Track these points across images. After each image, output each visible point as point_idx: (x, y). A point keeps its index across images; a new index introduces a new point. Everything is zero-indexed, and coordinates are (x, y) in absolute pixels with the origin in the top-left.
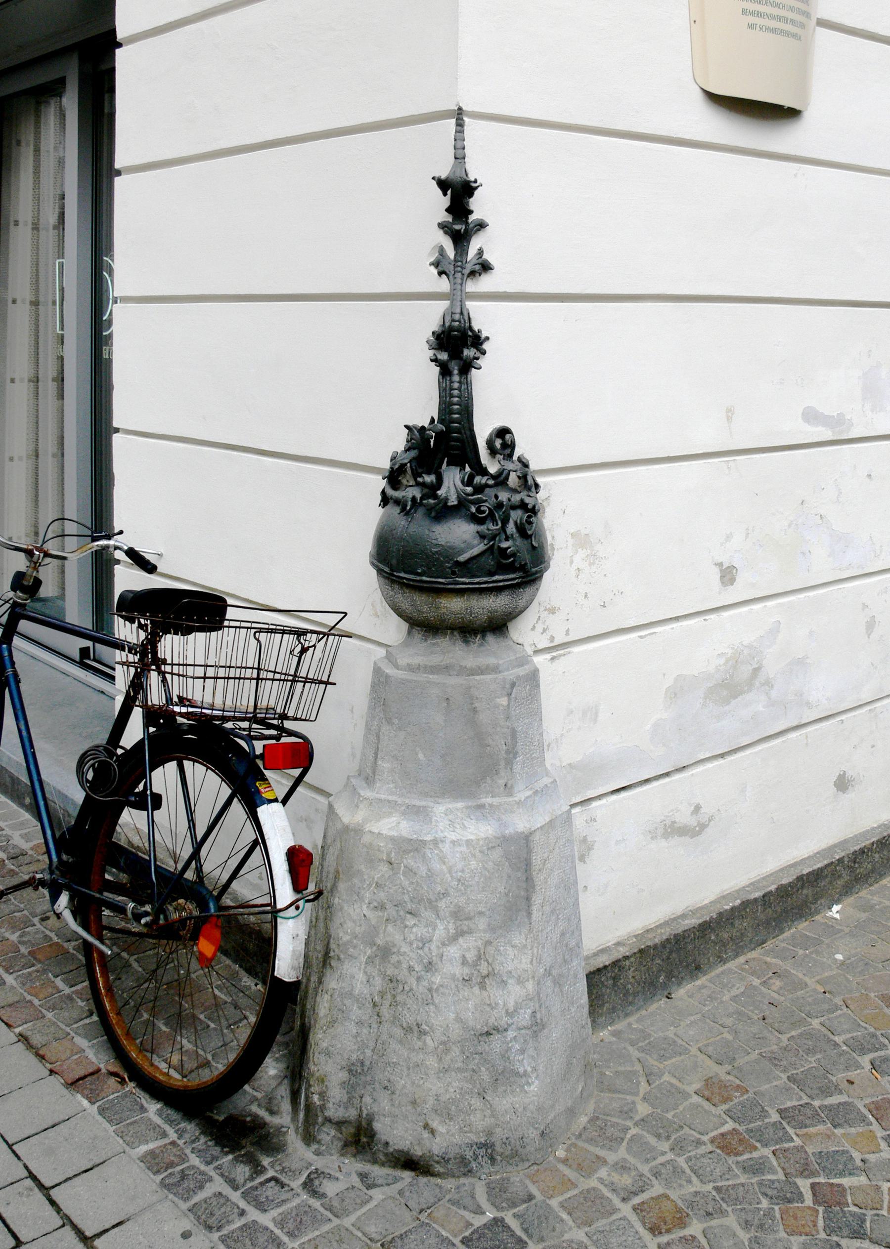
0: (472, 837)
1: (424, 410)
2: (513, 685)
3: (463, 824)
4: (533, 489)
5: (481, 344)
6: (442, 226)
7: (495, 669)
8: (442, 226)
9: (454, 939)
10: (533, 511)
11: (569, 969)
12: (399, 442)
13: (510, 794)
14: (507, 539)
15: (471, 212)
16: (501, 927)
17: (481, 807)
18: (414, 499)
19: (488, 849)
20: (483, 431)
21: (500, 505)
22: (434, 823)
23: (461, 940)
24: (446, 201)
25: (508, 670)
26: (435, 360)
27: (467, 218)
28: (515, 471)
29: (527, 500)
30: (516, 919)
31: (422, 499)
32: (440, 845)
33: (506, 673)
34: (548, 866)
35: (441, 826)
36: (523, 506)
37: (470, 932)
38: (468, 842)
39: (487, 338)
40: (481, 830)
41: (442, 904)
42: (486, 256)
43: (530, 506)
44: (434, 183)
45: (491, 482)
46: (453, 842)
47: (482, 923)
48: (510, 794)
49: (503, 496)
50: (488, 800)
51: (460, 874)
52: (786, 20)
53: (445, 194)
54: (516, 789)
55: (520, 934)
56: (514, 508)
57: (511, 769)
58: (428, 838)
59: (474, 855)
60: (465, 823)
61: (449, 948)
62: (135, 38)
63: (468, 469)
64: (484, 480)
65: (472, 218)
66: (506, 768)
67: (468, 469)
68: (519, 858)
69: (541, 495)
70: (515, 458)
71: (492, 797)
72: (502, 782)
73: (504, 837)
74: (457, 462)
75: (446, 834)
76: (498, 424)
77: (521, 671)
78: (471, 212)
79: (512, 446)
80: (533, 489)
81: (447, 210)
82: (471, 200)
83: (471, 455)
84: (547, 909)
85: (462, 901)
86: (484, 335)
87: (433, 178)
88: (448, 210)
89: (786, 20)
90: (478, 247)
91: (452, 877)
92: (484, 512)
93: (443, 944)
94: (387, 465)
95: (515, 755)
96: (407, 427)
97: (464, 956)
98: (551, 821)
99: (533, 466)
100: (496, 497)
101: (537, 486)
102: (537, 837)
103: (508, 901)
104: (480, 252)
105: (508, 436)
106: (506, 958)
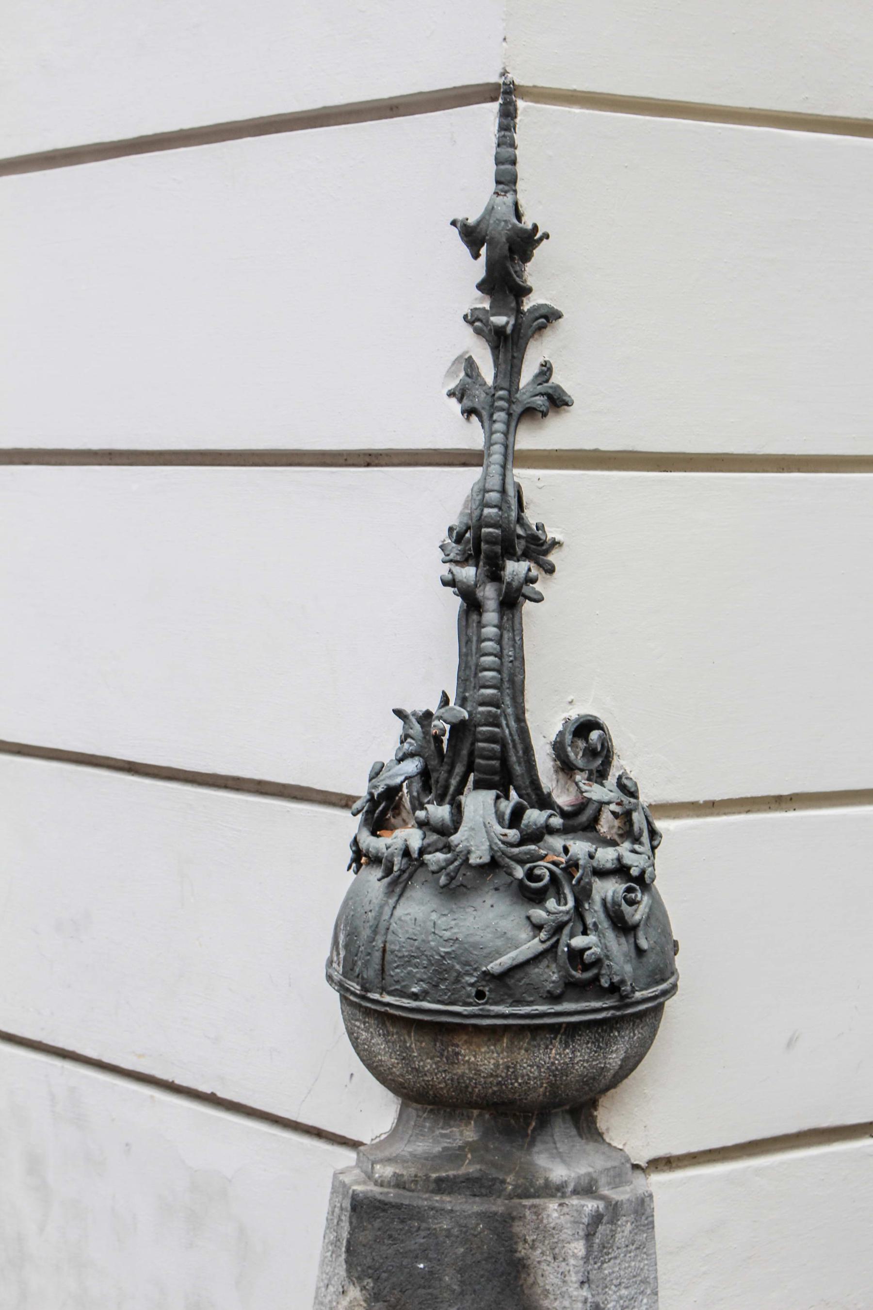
1: (428, 674)
5: (546, 552)
20: (545, 725)
44: (455, 231)
53: (476, 256)
56: (601, 873)
82: (529, 266)
87: (454, 223)
92: (539, 878)
104: (546, 370)
105: (594, 735)
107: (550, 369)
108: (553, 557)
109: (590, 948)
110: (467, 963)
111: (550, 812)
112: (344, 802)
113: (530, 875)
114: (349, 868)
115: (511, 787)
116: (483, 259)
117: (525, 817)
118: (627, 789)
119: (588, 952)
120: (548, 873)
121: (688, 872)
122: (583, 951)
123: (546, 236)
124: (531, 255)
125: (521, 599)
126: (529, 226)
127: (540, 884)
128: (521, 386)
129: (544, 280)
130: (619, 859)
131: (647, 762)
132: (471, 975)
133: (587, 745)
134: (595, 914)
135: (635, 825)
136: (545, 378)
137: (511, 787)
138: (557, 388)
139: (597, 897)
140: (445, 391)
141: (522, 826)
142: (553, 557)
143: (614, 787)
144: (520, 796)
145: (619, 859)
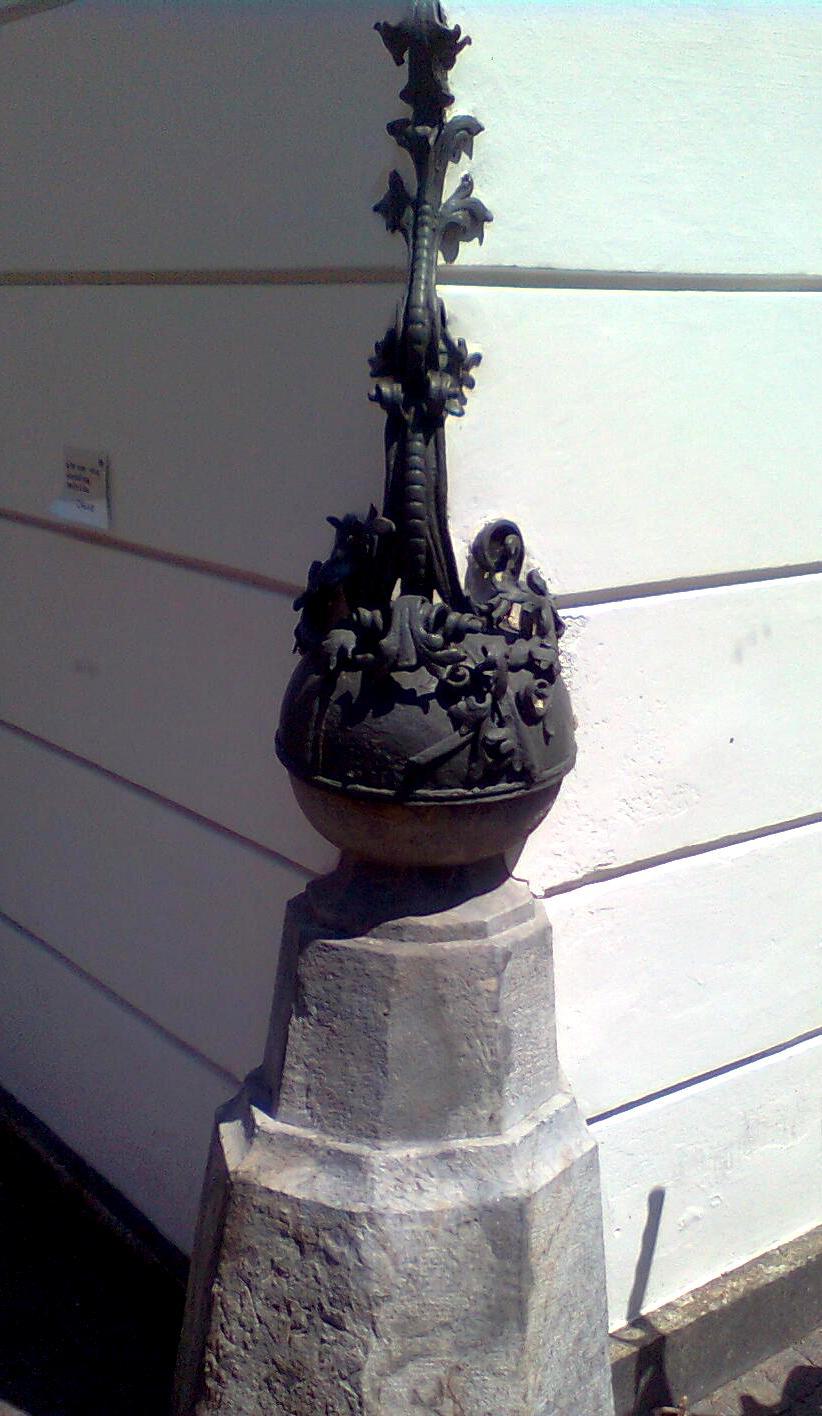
0: (429, 1208)
1: (362, 490)
2: (507, 956)
3: (418, 1184)
4: (552, 633)
5: (467, 368)
6: (395, 128)
7: (480, 931)
8: (395, 128)
9: (397, 1366)
10: (549, 675)
11: (586, 1390)
12: (322, 546)
13: (498, 1132)
14: (501, 724)
15: (450, 100)
16: (475, 1346)
17: (448, 1155)
18: (343, 650)
19: (458, 1225)
20: (464, 531)
21: (491, 664)
22: (369, 1183)
23: (411, 1367)
24: (401, 76)
25: (500, 931)
26: (379, 397)
27: (441, 114)
28: (521, 602)
29: (540, 653)
30: (501, 1334)
31: (355, 652)
32: (379, 1221)
33: (496, 936)
34: (557, 1243)
35: (379, 1190)
36: (531, 664)
37: (426, 1353)
38: (427, 1217)
39: (477, 359)
40: (449, 1195)
41: (381, 1314)
42: (477, 194)
43: (544, 666)
44: (378, 36)
45: (478, 624)
46: (401, 1217)
47: (445, 1340)
48: (498, 1132)
49: (497, 648)
50: (462, 1143)
51: (410, 1265)
52: (436, 550)
53: (399, 62)
54: (507, 1123)
55: (507, 1354)
56: (515, 668)
57: (500, 1092)
58: (359, 1208)
59: (434, 1236)
60: (421, 1182)
61: (390, 1380)
62: (816, 821)
63: (437, 599)
64: (466, 619)
65: (451, 114)
66: (491, 1091)
67: (437, 599)
68: (505, 1231)
69: (567, 644)
70: (522, 578)
71: (469, 1136)
72: (484, 1113)
73: (484, 1207)
74: (419, 587)
75: (389, 1202)
76: (493, 516)
77: (525, 930)
78: (450, 100)
79: (520, 555)
80: (552, 633)
81: (404, 95)
82: (451, 74)
83: (442, 575)
84: (554, 1309)
85: (412, 1307)
86: (472, 349)
87: (377, 26)
88: (405, 95)
89: (436, 550)
90: (462, 175)
91: (398, 1271)
92: (462, 677)
93: (381, 1374)
94: (303, 582)
95: (509, 1068)
96: (332, 520)
97: (415, 1391)
98: (563, 1172)
99: (553, 589)
100: (485, 651)
101: (559, 626)
102: (538, 1205)
103: (489, 1307)
104: (467, 184)
105: (510, 540)
106: (482, 1393)
107: (471, 184)
108: (473, 372)
109: (504, 740)
110: (395, 753)
111: (471, 615)
112: (227, 1075)
113: (453, 675)
114: (295, 651)
115: (435, 592)
116: (406, 65)
117: (448, 620)
118: (536, 587)
119: (504, 743)
120: (467, 672)
121: (594, 661)
122: (500, 742)
123: (468, 41)
124: (453, 61)
125: (444, 413)
126: (451, 27)
127: (461, 683)
128: (444, 201)
129: (467, 89)
130: (530, 654)
131: (553, 559)
132: (399, 764)
133: (501, 545)
134: (507, 706)
135: (542, 622)
136: (466, 193)
137: (435, 592)
138: (478, 203)
139: (511, 692)
140: (328, 515)
141: (437, 681)
142: (473, 372)
143: (526, 587)
144: (444, 599)
145: (530, 654)
